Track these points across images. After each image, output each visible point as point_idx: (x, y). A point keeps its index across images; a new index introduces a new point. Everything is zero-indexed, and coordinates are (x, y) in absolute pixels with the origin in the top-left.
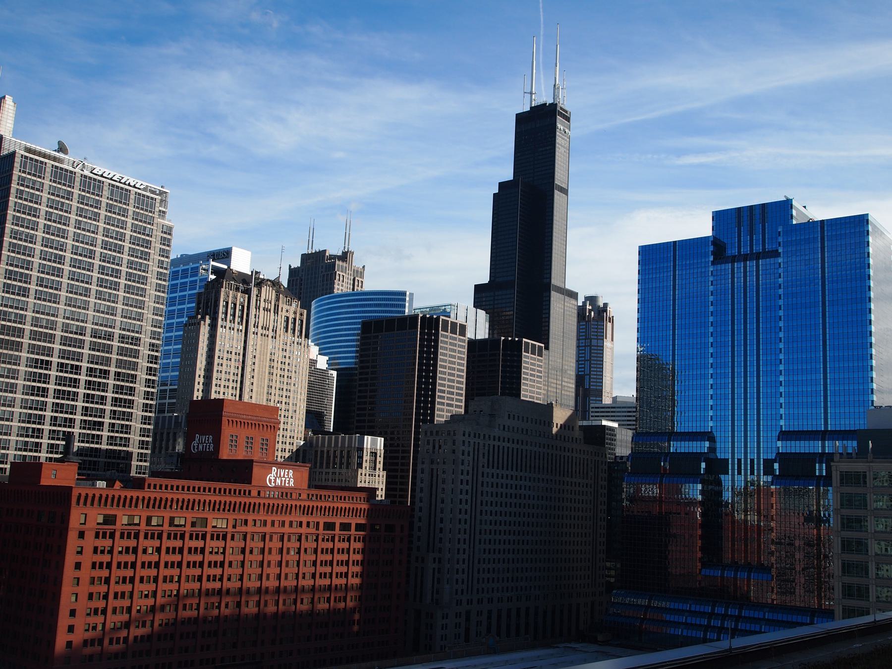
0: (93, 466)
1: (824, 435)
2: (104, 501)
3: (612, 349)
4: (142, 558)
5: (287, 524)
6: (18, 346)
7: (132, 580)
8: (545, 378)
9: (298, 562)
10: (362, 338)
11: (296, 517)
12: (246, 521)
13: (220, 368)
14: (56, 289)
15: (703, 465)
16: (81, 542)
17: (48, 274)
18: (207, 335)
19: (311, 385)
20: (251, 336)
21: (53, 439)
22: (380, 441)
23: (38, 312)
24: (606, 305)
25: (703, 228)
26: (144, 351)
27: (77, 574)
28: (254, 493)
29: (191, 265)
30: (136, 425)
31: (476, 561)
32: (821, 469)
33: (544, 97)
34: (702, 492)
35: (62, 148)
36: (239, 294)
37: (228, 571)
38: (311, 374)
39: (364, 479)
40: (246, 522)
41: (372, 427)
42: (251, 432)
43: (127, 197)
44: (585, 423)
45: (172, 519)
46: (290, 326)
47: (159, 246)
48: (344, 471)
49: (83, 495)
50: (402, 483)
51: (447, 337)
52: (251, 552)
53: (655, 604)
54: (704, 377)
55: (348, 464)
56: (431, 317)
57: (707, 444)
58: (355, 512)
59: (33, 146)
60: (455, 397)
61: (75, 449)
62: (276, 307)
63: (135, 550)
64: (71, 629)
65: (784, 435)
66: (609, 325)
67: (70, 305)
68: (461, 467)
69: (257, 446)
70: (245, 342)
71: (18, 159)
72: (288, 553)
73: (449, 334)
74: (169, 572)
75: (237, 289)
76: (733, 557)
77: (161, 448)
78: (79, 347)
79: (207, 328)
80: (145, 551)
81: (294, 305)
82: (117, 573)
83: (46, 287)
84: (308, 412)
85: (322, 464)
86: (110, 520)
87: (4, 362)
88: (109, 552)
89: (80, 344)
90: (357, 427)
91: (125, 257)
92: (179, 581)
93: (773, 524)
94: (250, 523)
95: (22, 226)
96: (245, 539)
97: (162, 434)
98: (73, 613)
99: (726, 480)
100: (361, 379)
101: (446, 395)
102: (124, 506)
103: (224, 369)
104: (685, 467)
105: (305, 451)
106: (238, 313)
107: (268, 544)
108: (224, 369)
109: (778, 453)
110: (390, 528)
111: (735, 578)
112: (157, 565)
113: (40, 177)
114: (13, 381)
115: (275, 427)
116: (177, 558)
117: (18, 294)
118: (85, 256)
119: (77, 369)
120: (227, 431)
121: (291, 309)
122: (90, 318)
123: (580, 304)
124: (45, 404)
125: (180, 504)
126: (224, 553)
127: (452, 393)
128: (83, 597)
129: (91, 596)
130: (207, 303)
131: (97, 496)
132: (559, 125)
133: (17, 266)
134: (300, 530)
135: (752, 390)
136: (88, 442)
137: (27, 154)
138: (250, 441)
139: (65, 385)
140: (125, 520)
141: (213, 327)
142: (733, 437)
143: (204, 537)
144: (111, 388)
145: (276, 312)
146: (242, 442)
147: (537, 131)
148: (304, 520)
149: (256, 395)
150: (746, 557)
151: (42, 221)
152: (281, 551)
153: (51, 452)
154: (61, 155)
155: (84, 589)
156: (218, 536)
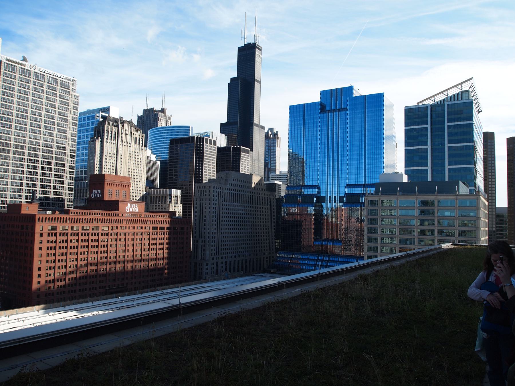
0: (47, 204)
1: (364, 186)
2: (51, 220)
3: (280, 151)
4: (70, 244)
5: (136, 228)
6: (8, 151)
7: (66, 254)
8: (251, 163)
9: (141, 244)
10: (170, 147)
11: (140, 225)
12: (117, 227)
13: (106, 161)
14: (25, 125)
15: (315, 199)
16: (41, 238)
17: (20, 118)
18: (99, 146)
19: (148, 167)
20: (120, 146)
21: (28, 193)
22: (179, 191)
23: (17, 136)
24: (277, 132)
25: (317, 98)
26: (68, 153)
27: (41, 252)
28: (120, 215)
29: (92, 114)
30: (66, 186)
31: (220, 241)
32: (362, 200)
33: (250, 40)
34: (315, 210)
35: (24, 59)
36: (114, 127)
37: (110, 249)
38: (148, 163)
39: (172, 208)
40: (117, 228)
41: (176, 186)
42: (118, 188)
43: (57, 82)
44: (268, 182)
45: (83, 227)
46: (138, 141)
47: (73, 105)
48: (163, 204)
49: (41, 218)
50: (189, 209)
51: (207, 146)
52: (120, 240)
53: (294, 256)
54: (316, 162)
55: (165, 201)
56: (201, 137)
57: (317, 190)
58: (165, 222)
59: (10, 58)
60: (211, 172)
61: (38, 198)
62: (131, 133)
63: (67, 241)
64: (39, 276)
65: (349, 186)
66: (279, 140)
67: (32, 132)
68: (213, 202)
69: (121, 194)
70: (117, 149)
71: (3, 64)
72: (137, 240)
73: (208, 144)
74: (83, 250)
75: (113, 125)
76: (327, 236)
77: (78, 196)
78: (37, 151)
79: (100, 143)
80: (71, 241)
81: (139, 132)
82: (59, 251)
83: (20, 124)
84: (147, 180)
85: (153, 202)
86: (54, 228)
87: (2, 159)
88: (55, 242)
89: (38, 150)
90: (169, 186)
91: (57, 110)
92: (88, 254)
93: (343, 223)
94: (119, 228)
95: (7, 96)
96: (117, 235)
97: (81, 190)
98: (40, 269)
99: (324, 205)
100: (170, 165)
101: (207, 171)
102: (60, 222)
103: (108, 161)
104: (308, 200)
105: (146, 196)
106: (113, 136)
107: (136, 237)
108: (108, 161)
109: (345, 194)
110: (178, 228)
111: (327, 245)
112: (77, 247)
113: (14, 73)
114: (7, 167)
115: (129, 186)
116: (86, 244)
117: (7, 128)
118: (38, 110)
119: (37, 161)
120: (107, 188)
121: (138, 134)
122: (42, 138)
123: (266, 132)
124: (22, 177)
125: (86, 220)
126: (107, 241)
127: (210, 170)
128: (44, 262)
129: (47, 262)
130: (99, 132)
131: (48, 218)
132: (256, 53)
133: (5, 114)
134: (142, 230)
135: (335, 168)
136: (44, 194)
137: (7, 62)
138: (118, 192)
139: (31, 169)
140: (61, 228)
141: (102, 142)
142: (327, 187)
143: (98, 235)
144: (53, 170)
145: (131, 135)
146: (114, 192)
147: (247, 54)
148: (144, 226)
149: (123, 172)
150: (332, 236)
151: (16, 94)
152: (133, 239)
153: (27, 199)
154: (24, 63)
155: (44, 259)
156: (105, 234)
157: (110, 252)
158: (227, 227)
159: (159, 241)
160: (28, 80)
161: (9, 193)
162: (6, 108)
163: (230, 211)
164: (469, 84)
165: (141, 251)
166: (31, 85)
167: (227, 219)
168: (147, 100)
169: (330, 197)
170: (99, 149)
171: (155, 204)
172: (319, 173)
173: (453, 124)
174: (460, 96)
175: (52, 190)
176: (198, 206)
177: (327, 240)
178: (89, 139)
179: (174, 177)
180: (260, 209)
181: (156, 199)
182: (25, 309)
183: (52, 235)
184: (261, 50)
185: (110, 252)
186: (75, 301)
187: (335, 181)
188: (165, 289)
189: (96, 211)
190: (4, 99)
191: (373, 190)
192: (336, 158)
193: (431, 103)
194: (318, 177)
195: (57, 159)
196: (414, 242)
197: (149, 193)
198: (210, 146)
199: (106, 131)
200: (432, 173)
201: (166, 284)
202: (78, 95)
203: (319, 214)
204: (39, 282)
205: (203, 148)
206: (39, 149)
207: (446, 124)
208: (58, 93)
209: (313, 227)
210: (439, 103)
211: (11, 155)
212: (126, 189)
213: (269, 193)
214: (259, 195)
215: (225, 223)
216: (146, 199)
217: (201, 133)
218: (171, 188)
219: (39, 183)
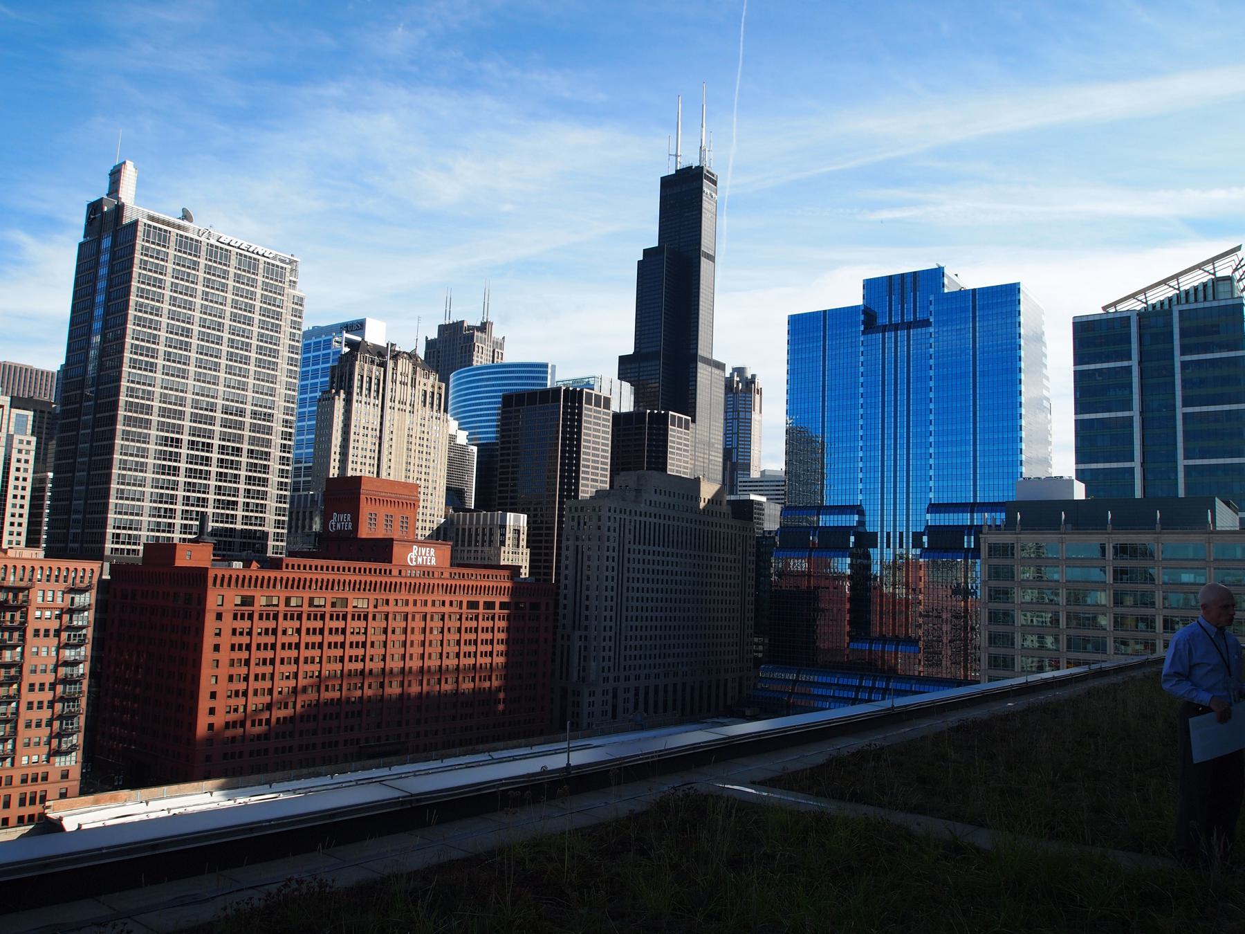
1: (973, 507)
2: (241, 581)
3: (760, 421)
4: (282, 639)
5: (429, 603)
7: (272, 662)
8: (692, 451)
11: (439, 596)
14: (184, 364)
15: (852, 539)
16: (219, 624)
18: (342, 411)
20: (387, 411)
21: (186, 519)
22: (523, 518)
24: (754, 376)
25: (855, 298)
26: (278, 427)
27: (217, 656)
28: (395, 572)
29: (324, 338)
32: (969, 542)
35: (186, 216)
39: (507, 556)
41: (514, 504)
42: (391, 510)
43: (256, 267)
44: (733, 498)
45: (311, 599)
46: (428, 400)
48: (486, 549)
49: (220, 576)
51: (590, 410)
52: (393, 632)
53: (803, 678)
54: (854, 449)
55: (491, 541)
56: (575, 390)
57: (856, 517)
58: (499, 590)
59: (157, 214)
63: (275, 632)
65: (934, 508)
66: (757, 397)
69: (397, 524)
70: (382, 417)
71: (140, 228)
72: (431, 632)
73: (593, 407)
74: (309, 653)
75: (372, 362)
77: (297, 527)
80: (284, 632)
81: (432, 378)
82: (256, 655)
84: (448, 489)
85: (463, 541)
86: (247, 601)
90: (500, 504)
91: (256, 329)
92: (320, 662)
93: (921, 597)
94: (392, 602)
96: (387, 619)
98: (213, 695)
99: (875, 553)
101: (590, 470)
103: (360, 445)
104: (834, 541)
105: (445, 529)
106: (373, 387)
108: (360, 445)
112: (298, 646)
115: (414, 505)
117: (146, 370)
120: (366, 509)
121: (429, 382)
123: (728, 375)
126: (365, 633)
129: (231, 678)
131: (234, 577)
132: (705, 189)
133: (143, 340)
134: (443, 610)
135: (902, 463)
138: (389, 519)
140: (263, 601)
141: (348, 402)
144: (244, 466)
145: (413, 385)
146: (382, 520)
147: (683, 195)
148: (447, 598)
149: (394, 471)
151: (168, 293)
154: (185, 223)
155: (224, 671)
156: (359, 616)
157: (371, 660)
158: (639, 604)
159: (482, 636)
160: (195, 262)
161: (145, 519)
162: (144, 326)
163: (646, 566)
164: (1233, 260)
165: (441, 658)
166: (201, 274)
167: (640, 585)
168: (449, 303)
169: (888, 534)
170: (341, 418)
171: (466, 548)
172: (860, 475)
173: (1195, 357)
174: (1210, 291)
175: (240, 513)
176: (571, 553)
177: (883, 639)
178: (318, 394)
179: (511, 483)
180: (717, 563)
181: (470, 535)
182: (182, 786)
183: (242, 618)
184: (715, 183)
185: (371, 660)
186: (293, 772)
187: (902, 496)
188: (495, 750)
189: (342, 563)
190: (141, 305)
191: (1000, 517)
192: (902, 441)
193: (1138, 308)
194: (860, 486)
195: (252, 441)
196: (1105, 644)
197: (452, 521)
198: (596, 411)
199: (357, 377)
200: (1144, 478)
201: (497, 739)
202: (301, 294)
203: (861, 572)
204: (211, 726)
205: (580, 414)
206: (150, 408)
207: (1178, 359)
208: (259, 291)
209: (848, 606)
210: (1158, 306)
211: (153, 432)
212: (407, 512)
213: (738, 523)
214: (714, 529)
215: (635, 595)
216: (445, 534)
217: (575, 381)
218: (506, 511)
219: (211, 497)
